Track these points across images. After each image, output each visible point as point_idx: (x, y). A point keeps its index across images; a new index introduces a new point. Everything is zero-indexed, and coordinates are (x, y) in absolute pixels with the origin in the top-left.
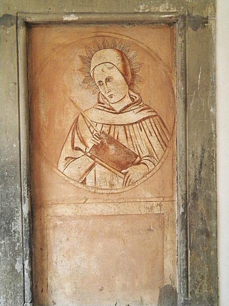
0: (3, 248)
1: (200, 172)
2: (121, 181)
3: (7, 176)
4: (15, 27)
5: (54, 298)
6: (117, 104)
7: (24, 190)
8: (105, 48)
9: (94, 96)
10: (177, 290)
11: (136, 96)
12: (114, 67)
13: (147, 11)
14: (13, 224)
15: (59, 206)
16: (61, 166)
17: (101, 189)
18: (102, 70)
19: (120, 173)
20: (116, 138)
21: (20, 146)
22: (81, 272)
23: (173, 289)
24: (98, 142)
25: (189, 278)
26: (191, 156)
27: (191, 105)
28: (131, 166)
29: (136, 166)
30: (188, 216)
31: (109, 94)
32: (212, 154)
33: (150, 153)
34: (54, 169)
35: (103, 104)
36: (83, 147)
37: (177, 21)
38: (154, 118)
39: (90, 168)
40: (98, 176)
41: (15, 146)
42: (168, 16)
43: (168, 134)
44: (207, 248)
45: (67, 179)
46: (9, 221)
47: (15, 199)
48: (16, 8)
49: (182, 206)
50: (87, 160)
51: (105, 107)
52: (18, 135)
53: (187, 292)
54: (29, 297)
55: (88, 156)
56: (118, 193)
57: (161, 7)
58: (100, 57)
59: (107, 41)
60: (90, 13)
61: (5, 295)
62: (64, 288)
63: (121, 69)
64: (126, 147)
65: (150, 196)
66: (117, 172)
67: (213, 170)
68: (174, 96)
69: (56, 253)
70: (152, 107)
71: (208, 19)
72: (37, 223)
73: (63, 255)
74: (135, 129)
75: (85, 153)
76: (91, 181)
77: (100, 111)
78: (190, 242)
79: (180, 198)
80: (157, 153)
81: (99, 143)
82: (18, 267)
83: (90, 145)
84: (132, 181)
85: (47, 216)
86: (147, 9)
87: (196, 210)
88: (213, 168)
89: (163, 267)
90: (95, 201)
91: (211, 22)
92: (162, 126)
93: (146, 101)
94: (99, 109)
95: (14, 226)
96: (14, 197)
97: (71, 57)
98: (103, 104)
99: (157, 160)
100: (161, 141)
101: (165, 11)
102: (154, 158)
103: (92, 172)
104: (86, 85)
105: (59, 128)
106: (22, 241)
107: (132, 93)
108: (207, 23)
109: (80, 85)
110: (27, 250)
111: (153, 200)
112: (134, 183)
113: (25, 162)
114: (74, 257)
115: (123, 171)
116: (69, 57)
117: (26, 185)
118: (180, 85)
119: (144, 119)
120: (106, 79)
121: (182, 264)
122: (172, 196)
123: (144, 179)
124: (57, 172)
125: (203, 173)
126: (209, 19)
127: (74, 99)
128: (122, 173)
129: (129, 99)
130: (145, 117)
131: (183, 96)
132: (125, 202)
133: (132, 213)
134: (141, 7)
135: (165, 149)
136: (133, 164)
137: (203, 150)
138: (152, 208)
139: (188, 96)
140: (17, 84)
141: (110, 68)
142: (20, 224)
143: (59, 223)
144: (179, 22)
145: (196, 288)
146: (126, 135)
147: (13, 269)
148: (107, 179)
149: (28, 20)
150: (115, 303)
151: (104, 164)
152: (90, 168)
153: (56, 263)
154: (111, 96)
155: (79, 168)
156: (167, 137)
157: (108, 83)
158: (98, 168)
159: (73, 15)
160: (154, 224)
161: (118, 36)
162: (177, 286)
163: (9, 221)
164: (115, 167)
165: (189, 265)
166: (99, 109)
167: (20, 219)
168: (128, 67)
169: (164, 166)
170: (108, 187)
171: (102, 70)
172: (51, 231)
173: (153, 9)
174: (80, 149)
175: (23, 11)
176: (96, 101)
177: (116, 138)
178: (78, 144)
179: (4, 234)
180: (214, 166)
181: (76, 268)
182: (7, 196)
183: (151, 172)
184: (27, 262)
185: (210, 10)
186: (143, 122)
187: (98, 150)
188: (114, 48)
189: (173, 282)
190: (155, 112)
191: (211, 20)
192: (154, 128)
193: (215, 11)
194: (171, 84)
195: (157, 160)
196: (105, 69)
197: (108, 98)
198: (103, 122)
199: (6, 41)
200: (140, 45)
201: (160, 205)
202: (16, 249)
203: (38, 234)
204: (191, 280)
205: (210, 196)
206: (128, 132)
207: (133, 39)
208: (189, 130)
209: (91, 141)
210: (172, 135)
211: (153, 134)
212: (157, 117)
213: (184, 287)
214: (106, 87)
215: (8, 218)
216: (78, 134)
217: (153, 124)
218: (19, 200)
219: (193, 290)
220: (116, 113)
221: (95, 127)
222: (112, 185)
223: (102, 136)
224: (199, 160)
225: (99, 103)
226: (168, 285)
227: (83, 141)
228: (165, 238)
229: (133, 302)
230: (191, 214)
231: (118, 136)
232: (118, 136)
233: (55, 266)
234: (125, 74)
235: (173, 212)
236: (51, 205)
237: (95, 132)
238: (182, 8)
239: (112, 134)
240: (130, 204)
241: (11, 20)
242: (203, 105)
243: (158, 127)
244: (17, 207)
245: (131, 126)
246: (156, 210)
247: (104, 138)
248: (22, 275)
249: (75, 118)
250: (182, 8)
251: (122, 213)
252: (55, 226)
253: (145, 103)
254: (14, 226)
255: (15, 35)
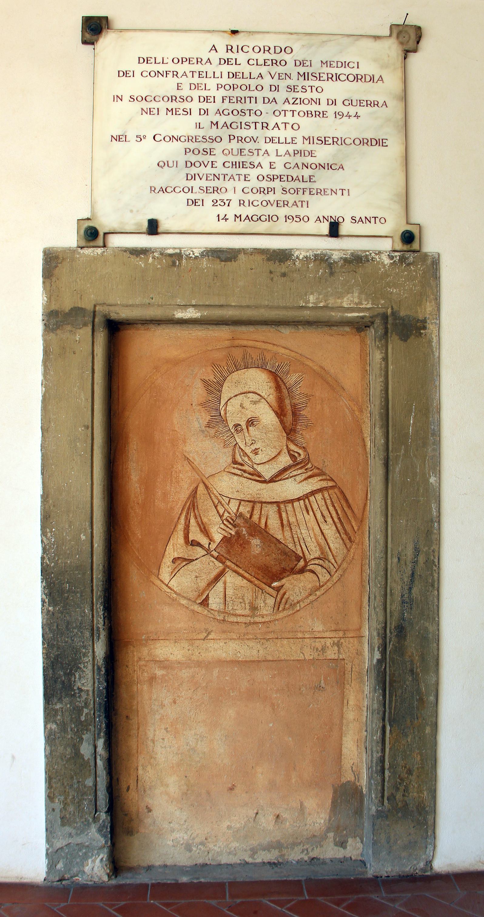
0: (59, 717)
1: (410, 589)
2: (271, 601)
3: (69, 591)
4: (90, 328)
5: (149, 801)
6: (267, 466)
7: (98, 616)
8: (246, 367)
9: (226, 450)
10: (364, 790)
11: (300, 451)
12: (263, 400)
13: (321, 305)
14: (77, 676)
15: (158, 644)
16: (165, 574)
17: (236, 615)
18: (241, 406)
19: (270, 586)
20: (263, 525)
21: (92, 537)
22: (198, 759)
23: (357, 787)
24: (231, 531)
25: (387, 773)
26: (395, 560)
27: (397, 469)
28: (288, 576)
29: (299, 576)
30: (388, 665)
31: (253, 447)
32: (432, 558)
33: (322, 553)
34: (153, 579)
35: (242, 465)
36: (204, 541)
37: (373, 323)
38: (331, 491)
39: (217, 579)
40: (230, 592)
41: (83, 537)
42: (149, 890)
43: (355, 521)
44: (420, 720)
45: (175, 595)
46: (71, 670)
47: (82, 632)
48: (92, 296)
49: (379, 648)
50: (211, 564)
51: (245, 471)
52: (90, 520)
53: (383, 797)
54: (104, 802)
55: (213, 556)
56: (264, 622)
57: (345, 299)
58: (238, 382)
59: (250, 356)
60: (221, 306)
61: (62, 798)
62: (167, 785)
63: (274, 404)
64: (281, 543)
65: (321, 628)
66: (264, 586)
67: (433, 586)
68: (366, 453)
69: (154, 724)
70: (327, 472)
71: (426, 322)
72: (121, 672)
73: (166, 729)
74: (298, 510)
75: (208, 552)
76: (218, 600)
77: (236, 478)
78: (390, 713)
79: (375, 634)
80: (334, 552)
81: (233, 533)
82: (86, 750)
83: (218, 538)
84: (290, 602)
85: (138, 661)
86: (321, 302)
87: (402, 655)
88: (433, 581)
89: (341, 750)
90: (224, 636)
91: (431, 327)
92: (344, 505)
93: (317, 460)
94: (235, 474)
95: (80, 679)
96: (80, 628)
97: (187, 381)
98: (242, 465)
99: (335, 564)
100: (342, 531)
101: (352, 306)
102: (329, 562)
103: (220, 585)
104: (212, 431)
105: (162, 505)
106: (92, 706)
107: (292, 447)
108: (425, 328)
109: (203, 431)
110: (101, 722)
111: (327, 634)
112: (293, 605)
113: (101, 567)
114: (184, 732)
115: (275, 584)
116: (183, 382)
117: (102, 607)
118: (377, 434)
119: (313, 493)
120: (248, 422)
121: (374, 749)
122: (359, 629)
123: (311, 598)
124: (158, 582)
125: (415, 591)
126: (428, 321)
127: (191, 455)
128: (273, 588)
129: (288, 458)
130: (315, 489)
131: (382, 455)
132: (277, 638)
133: (289, 658)
134: (312, 298)
135: (348, 547)
136: (293, 571)
137: (417, 551)
138: (324, 649)
139: (391, 454)
140: (90, 429)
141: (255, 403)
142: (90, 675)
143: (159, 673)
144: (376, 325)
145: (397, 789)
146: (281, 520)
147: (77, 754)
148: (246, 600)
149: (114, 316)
150: (255, 811)
151: (241, 571)
152: (217, 579)
153: (154, 743)
154: (256, 452)
155: (196, 577)
156: (353, 524)
157: (251, 428)
158: (230, 578)
159: (191, 310)
160: (325, 679)
161: (270, 347)
162: (364, 782)
163: (71, 670)
164: (260, 577)
165: (387, 750)
166: (235, 474)
167: (90, 667)
168: (287, 402)
169: (346, 575)
170: (247, 612)
171: (241, 406)
172: (145, 687)
173: (331, 302)
174: (199, 545)
175: (105, 301)
176: (230, 460)
177: (263, 525)
178: (195, 534)
179: (61, 693)
180: (436, 578)
181: (189, 751)
182: (67, 627)
183: (323, 586)
184: (101, 743)
185: (429, 307)
186: (312, 498)
187: (232, 547)
188: (262, 367)
189: (357, 776)
190: (332, 480)
191: (432, 323)
192: (331, 508)
193: (439, 310)
194: (361, 431)
195: (335, 564)
196: (247, 404)
197: (251, 455)
198: (242, 497)
199: (74, 353)
200: (307, 363)
201: (338, 645)
202: (83, 718)
203: (123, 692)
204: (389, 777)
205: (426, 629)
206: (284, 515)
207: (297, 353)
208: (392, 515)
209: (220, 530)
210: (361, 521)
211: (329, 520)
212: (336, 490)
213: (376, 789)
214: (246, 434)
215: (69, 665)
216: (196, 518)
217: (329, 502)
218: (87, 634)
219: (392, 794)
220: (265, 482)
221: (227, 507)
222: (254, 608)
223: (239, 521)
224: (409, 568)
225: (235, 462)
226: (349, 781)
227: (205, 531)
228: (345, 702)
229: (286, 809)
230: (393, 662)
231: (266, 523)
232: (266, 523)
233: (151, 748)
234: (280, 413)
235: (360, 657)
236: (147, 640)
237: (226, 514)
238: (383, 302)
239: (256, 517)
240: (285, 642)
241: (84, 316)
242: (418, 471)
243: (337, 508)
244: (84, 647)
245: (290, 505)
246: (331, 654)
247: (242, 525)
248: (92, 763)
249: (192, 488)
250: (383, 302)
251: (270, 658)
252: (152, 679)
253: (316, 465)
254: (80, 679)
255: (91, 343)
